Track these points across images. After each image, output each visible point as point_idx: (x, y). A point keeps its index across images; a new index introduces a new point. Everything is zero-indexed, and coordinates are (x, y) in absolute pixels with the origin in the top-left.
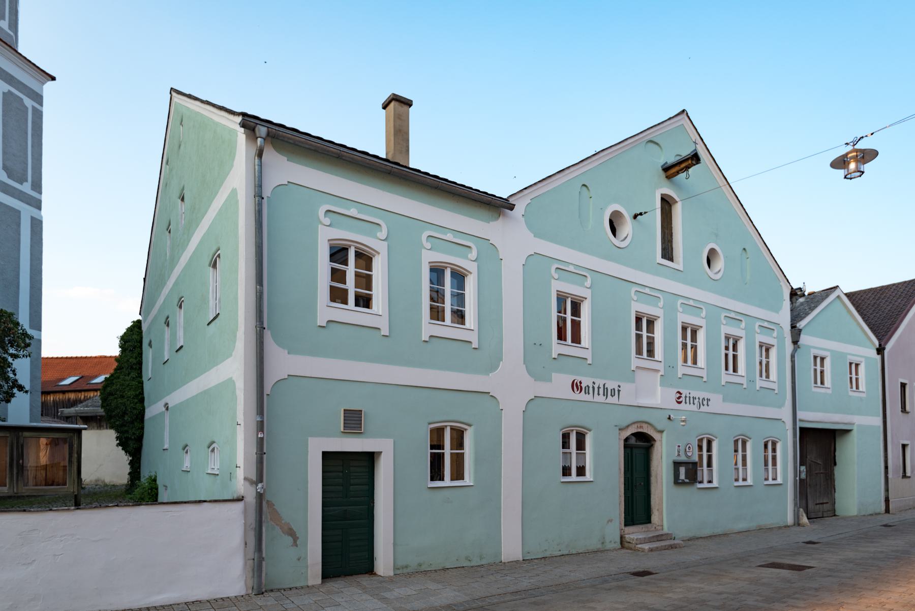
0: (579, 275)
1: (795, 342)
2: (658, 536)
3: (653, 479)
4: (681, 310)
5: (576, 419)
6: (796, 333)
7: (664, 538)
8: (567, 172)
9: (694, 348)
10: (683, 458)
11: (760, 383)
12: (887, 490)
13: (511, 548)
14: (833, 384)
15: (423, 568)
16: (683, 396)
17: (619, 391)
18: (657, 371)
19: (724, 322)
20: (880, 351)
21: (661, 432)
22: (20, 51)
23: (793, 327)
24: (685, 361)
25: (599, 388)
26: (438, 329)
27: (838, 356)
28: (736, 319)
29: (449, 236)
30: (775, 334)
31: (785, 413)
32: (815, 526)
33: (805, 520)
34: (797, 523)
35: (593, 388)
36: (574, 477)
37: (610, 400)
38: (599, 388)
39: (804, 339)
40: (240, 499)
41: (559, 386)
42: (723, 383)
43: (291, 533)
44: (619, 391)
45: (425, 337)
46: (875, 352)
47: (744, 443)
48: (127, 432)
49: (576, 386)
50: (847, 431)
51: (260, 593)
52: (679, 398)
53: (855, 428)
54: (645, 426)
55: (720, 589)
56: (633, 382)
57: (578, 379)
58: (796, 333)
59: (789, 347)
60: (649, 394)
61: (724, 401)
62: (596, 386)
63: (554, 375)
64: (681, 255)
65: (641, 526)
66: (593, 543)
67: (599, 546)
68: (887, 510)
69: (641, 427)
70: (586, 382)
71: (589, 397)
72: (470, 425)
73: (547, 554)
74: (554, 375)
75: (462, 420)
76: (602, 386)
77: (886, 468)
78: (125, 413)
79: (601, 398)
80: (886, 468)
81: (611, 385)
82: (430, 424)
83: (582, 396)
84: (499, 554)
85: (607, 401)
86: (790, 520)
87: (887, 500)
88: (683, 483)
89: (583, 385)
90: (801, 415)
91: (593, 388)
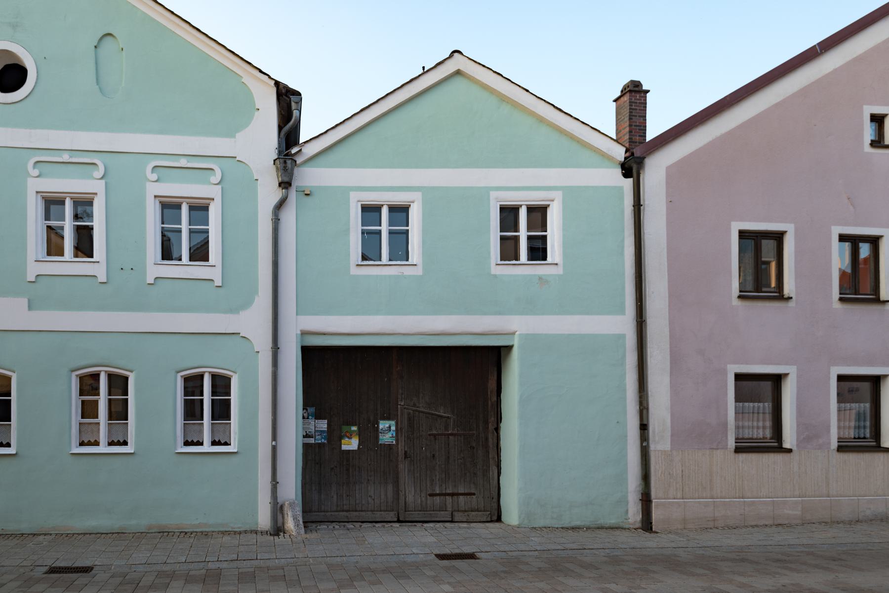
0: (81, 162)
12: (646, 477)
14: (565, 255)
26: (170, 270)
29: (66, 157)
31: (254, 323)
32: (313, 536)
45: (150, 280)
46: (618, 171)
53: (516, 342)
61: (30, 308)
68: (647, 525)
72: (131, 371)
75: (196, 365)
82: (178, 372)
84: (257, 524)
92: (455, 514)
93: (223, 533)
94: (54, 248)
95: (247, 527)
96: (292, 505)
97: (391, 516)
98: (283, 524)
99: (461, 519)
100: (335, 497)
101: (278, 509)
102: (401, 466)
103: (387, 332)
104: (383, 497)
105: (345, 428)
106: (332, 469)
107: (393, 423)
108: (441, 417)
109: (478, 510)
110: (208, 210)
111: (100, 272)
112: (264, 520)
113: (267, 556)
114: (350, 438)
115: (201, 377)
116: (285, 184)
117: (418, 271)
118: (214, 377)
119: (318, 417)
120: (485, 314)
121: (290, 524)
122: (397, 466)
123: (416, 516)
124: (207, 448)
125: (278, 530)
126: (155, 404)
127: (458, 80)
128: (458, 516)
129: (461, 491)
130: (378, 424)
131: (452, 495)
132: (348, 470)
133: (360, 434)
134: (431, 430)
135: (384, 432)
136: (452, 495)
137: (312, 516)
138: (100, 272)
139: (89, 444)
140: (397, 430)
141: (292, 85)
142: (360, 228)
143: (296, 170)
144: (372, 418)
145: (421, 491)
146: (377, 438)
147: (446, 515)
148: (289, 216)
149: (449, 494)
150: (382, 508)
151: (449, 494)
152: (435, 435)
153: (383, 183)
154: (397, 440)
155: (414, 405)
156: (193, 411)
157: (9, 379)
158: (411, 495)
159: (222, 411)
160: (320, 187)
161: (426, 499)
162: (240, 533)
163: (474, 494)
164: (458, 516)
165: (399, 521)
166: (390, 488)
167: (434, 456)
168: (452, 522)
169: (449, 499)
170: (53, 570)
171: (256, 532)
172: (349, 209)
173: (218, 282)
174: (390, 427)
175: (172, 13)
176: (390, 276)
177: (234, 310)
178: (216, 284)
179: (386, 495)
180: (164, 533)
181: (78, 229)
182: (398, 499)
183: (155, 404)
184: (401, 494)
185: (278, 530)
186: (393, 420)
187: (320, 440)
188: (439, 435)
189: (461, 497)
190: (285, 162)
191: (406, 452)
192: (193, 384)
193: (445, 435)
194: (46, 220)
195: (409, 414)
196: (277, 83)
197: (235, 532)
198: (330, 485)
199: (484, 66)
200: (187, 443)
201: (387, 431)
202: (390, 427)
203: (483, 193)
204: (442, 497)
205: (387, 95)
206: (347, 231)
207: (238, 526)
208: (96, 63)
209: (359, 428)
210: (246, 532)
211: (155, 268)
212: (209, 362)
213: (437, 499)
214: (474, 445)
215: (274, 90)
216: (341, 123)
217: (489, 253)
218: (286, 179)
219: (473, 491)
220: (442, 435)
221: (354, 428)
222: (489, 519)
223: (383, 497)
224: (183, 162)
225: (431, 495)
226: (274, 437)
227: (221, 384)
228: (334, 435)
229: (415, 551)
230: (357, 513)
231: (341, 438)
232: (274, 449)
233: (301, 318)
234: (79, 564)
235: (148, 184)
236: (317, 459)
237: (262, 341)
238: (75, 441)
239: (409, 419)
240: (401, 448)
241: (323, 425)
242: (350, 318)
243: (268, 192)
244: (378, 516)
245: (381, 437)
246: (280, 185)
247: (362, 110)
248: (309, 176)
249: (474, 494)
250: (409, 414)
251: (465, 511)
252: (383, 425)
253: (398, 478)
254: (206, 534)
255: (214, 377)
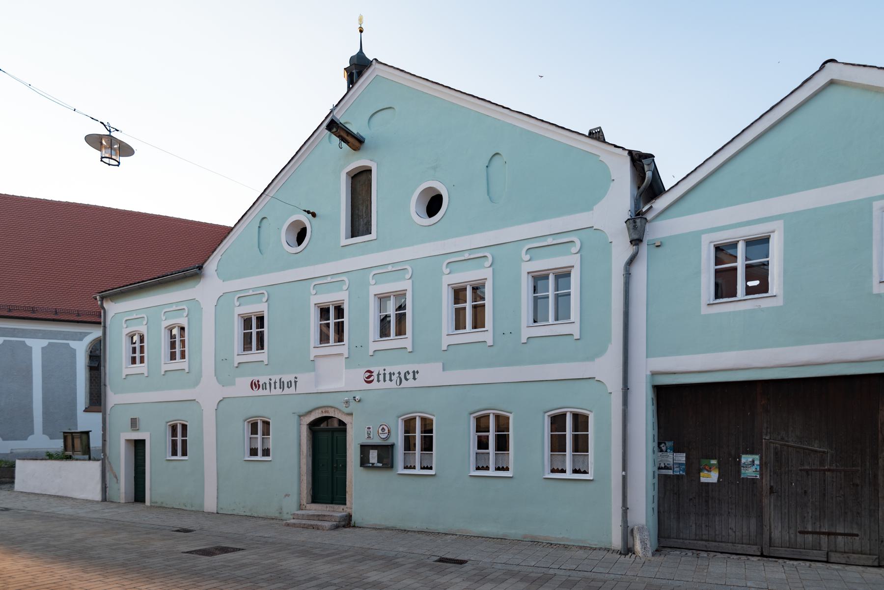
2: (319, 516)
5: (259, 411)
7: (326, 518)
8: (249, 213)
10: (376, 441)
13: (210, 504)
15: (164, 505)
16: (375, 374)
17: (296, 382)
18: (341, 354)
25: (275, 383)
29: (466, 256)
31: (607, 367)
35: (385, 374)
36: (259, 457)
37: (287, 391)
38: (275, 383)
41: (242, 387)
43: (116, 477)
44: (296, 382)
45: (524, 340)
49: (255, 385)
52: (369, 377)
54: (330, 410)
56: (314, 370)
57: (256, 379)
60: (333, 378)
61: (444, 369)
62: (272, 382)
63: (237, 380)
64: (231, 241)
65: (325, 505)
67: (277, 515)
69: (328, 412)
70: (263, 380)
71: (266, 392)
73: (235, 512)
74: (237, 380)
76: (278, 381)
79: (278, 391)
81: (286, 379)
83: (261, 392)
84: (611, 543)
85: (284, 393)
88: (373, 467)
89: (261, 383)
91: (385, 374)
92: (832, 554)
93: (581, 547)
94: (459, 324)
95: (602, 545)
96: (641, 529)
97: (754, 550)
98: (633, 546)
99: (839, 560)
100: (694, 526)
101: (628, 532)
102: (766, 501)
103: (742, 367)
104: (745, 530)
105: (704, 462)
106: (691, 499)
107: (757, 458)
108: (816, 451)
109: (861, 553)
110: (768, 242)
111: (575, 329)
112: (616, 541)
113: (601, 570)
114: (709, 471)
115: (564, 415)
116: (636, 241)
117: (779, 302)
118: (576, 416)
119: (676, 450)
120: (865, 339)
121: (638, 547)
122: (761, 501)
123: (782, 552)
124: (569, 475)
125: (628, 550)
126: (530, 439)
127: (833, 91)
128: (834, 557)
129: (840, 530)
130: (740, 458)
131: (829, 534)
132: (707, 501)
133: (720, 467)
134: (802, 465)
135: (746, 466)
136: (829, 534)
137: (666, 541)
138: (575, 329)
139: (410, 468)
140: (761, 465)
141: (644, 151)
142: (712, 267)
143: (648, 226)
144: (733, 452)
145: (789, 528)
146: (739, 472)
147: (814, 554)
148: (640, 270)
149: (824, 533)
150: (744, 541)
151: (824, 533)
152: (807, 471)
153: (732, 221)
154: (761, 475)
155: (782, 439)
156: (558, 445)
157: (508, 418)
158: (778, 532)
159: (581, 445)
160: (671, 237)
161: (796, 536)
162: (595, 549)
163: (857, 535)
164: (834, 557)
165: (762, 555)
166: (753, 522)
167: (805, 492)
168: (827, 562)
169: (824, 539)
170: (442, 560)
171: (608, 550)
172: (700, 252)
173: (577, 336)
174: (753, 461)
175: (542, 121)
176: (745, 311)
177: (591, 358)
178: (576, 337)
179: (749, 528)
180: (535, 542)
181: (475, 307)
182: (762, 534)
183: (530, 439)
184: (766, 529)
185: (628, 550)
186: (756, 454)
187: (678, 472)
188: (812, 470)
189: (840, 537)
190: (635, 222)
191: (771, 487)
192: (557, 421)
193: (820, 470)
194: (455, 303)
195: (776, 448)
196: (630, 152)
197: (591, 548)
198: (683, 514)
199: (865, 66)
200: (553, 471)
201: (750, 465)
202: (753, 461)
203: (696, 236)
204: (815, 536)
205: (743, 131)
206: (698, 273)
207: (594, 543)
208: (488, 180)
209: (719, 462)
210: (600, 549)
211: (528, 331)
212: (570, 404)
213: (810, 537)
214: (858, 482)
215: (628, 159)
216: (692, 172)
217: (871, 271)
218: (636, 237)
219: (855, 532)
220: (816, 470)
221: (714, 462)
222: (876, 564)
223: (745, 530)
224: (550, 241)
225: (800, 532)
226: (624, 468)
227: (581, 422)
228: (693, 469)
229: (749, 584)
230: (716, 544)
231: (700, 471)
232: (624, 478)
233: (651, 360)
234: (459, 558)
235: (523, 264)
236: (672, 492)
237: (614, 384)
238: (473, 466)
239: (776, 454)
240: (766, 483)
241: (682, 458)
242: (701, 356)
243: (622, 250)
244: (739, 548)
245: (743, 471)
246: (631, 242)
247: (715, 154)
248: (661, 228)
249: (857, 535)
250: (776, 448)
251: (845, 552)
252: (746, 459)
253: (762, 513)
254: (566, 547)
255: (576, 416)
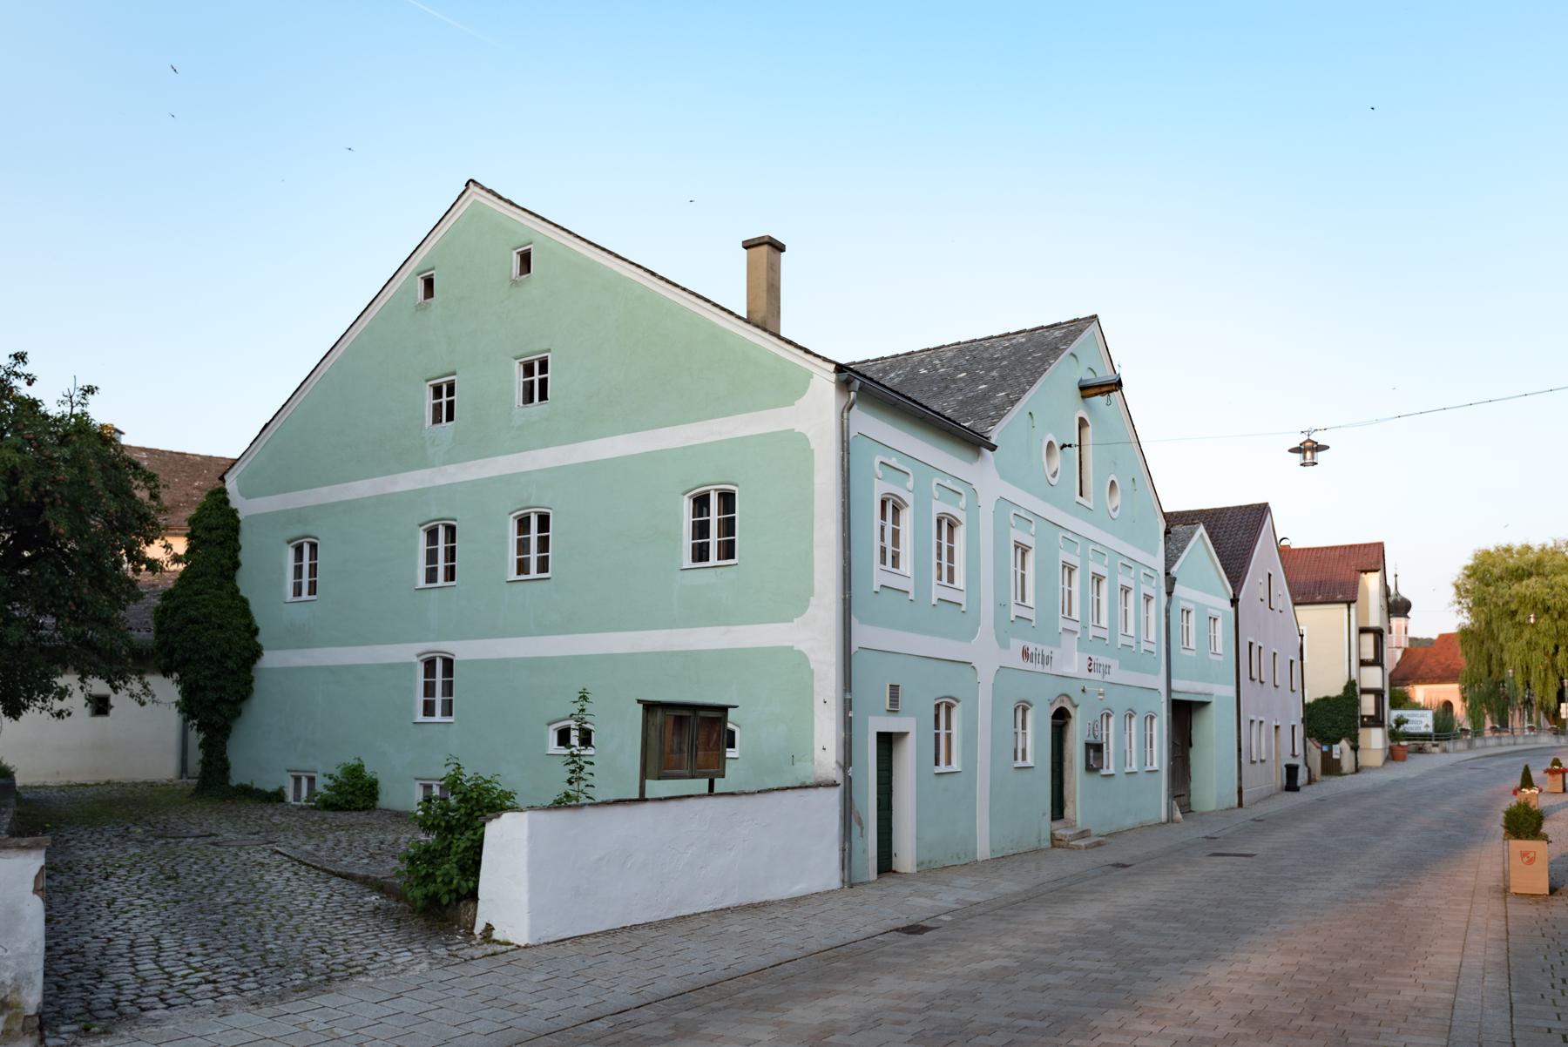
1: (1169, 593)
3: (1066, 764)
4: (936, 495)
6: (1171, 582)
9: (951, 551)
11: (937, 592)
12: (1240, 778)
19: (936, 495)
20: (1234, 602)
21: (1076, 707)
22: (783, 334)
23: (1167, 574)
24: (940, 578)
27: (1202, 608)
28: (1025, 519)
30: (963, 502)
33: (1178, 815)
34: (1171, 820)
39: (1179, 589)
40: (834, 784)
42: (934, 601)
47: (949, 708)
48: (223, 688)
50: (1204, 704)
51: (1053, 846)
53: (1214, 700)
55: (920, 986)
58: (1171, 582)
59: (1164, 598)
60: (1072, 663)
66: (1034, 844)
68: (1240, 804)
77: (1240, 750)
78: (225, 656)
80: (1240, 750)
83: (1029, 666)
84: (975, 852)
86: (1164, 816)
87: (1240, 791)
90: (1175, 684)
